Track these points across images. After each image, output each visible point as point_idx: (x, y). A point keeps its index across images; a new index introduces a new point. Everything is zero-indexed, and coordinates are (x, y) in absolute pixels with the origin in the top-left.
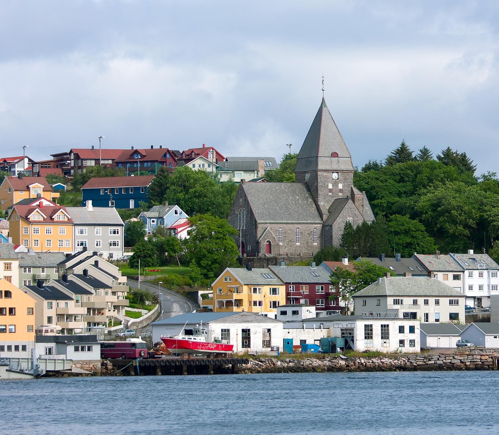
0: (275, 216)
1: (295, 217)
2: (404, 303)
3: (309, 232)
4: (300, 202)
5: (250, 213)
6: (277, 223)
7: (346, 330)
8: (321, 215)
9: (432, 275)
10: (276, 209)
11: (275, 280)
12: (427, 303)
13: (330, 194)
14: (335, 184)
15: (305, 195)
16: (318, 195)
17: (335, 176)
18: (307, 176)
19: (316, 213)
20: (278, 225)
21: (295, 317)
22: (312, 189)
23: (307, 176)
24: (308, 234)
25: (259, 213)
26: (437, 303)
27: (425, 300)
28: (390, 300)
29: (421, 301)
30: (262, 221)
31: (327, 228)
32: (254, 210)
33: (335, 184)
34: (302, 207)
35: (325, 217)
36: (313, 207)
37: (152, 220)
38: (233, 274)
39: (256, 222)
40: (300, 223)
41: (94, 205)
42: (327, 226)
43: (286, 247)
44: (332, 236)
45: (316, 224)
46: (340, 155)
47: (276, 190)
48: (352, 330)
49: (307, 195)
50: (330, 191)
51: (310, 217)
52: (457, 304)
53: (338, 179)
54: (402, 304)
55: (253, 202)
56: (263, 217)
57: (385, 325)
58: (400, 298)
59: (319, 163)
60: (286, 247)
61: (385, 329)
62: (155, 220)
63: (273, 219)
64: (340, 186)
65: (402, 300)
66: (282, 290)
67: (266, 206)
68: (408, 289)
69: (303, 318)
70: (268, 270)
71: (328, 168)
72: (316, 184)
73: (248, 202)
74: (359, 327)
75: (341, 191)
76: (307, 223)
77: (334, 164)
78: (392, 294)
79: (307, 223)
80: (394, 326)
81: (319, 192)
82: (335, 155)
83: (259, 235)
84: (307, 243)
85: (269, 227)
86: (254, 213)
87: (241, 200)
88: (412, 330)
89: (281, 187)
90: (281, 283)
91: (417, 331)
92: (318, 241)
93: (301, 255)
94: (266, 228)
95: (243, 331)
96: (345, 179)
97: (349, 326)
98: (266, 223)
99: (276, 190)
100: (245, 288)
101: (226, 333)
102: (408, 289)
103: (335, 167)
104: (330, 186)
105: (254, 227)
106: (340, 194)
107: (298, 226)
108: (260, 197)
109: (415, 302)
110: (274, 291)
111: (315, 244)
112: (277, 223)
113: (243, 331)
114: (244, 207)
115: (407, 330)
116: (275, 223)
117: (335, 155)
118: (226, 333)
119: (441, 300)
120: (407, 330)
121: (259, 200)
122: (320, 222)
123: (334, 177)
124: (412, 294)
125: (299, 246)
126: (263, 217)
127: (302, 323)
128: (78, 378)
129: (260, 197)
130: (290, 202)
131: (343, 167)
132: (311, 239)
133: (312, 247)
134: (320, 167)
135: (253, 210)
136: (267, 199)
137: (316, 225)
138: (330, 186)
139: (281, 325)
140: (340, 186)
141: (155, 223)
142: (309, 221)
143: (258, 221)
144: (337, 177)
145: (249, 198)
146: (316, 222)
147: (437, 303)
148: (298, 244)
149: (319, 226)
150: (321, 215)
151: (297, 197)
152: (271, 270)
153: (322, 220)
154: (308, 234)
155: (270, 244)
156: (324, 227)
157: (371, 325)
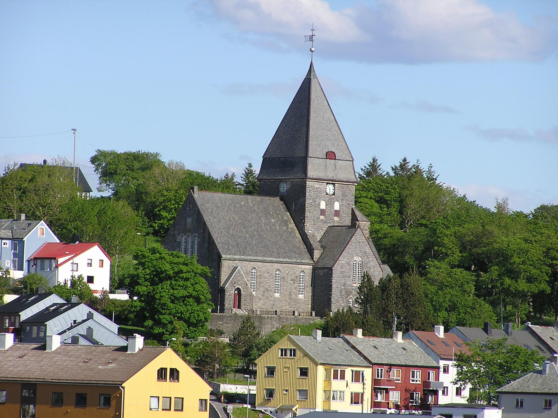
0: (246, 248)
1: (273, 252)
4: (278, 228)
8: (310, 250)
13: (322, 217)
14: (330, 204)
17: (330, 189)
19: (303, 247)
20: (251, 263)
24: (292, 280)
25: (223, 243)
27: (546, 401)
32: (215, 236)
33: (330, 204)
35: (317, 254)
36: (297, 238)
37: (4, 241)
39: (220, 257)
40: (281, 263)
43: (260, 299)
45: (304, 264)
50: (323, 212)
51: (295, 252)
52: (522, 406)
53: (334, 194)
55: (211, 224)
56: (228, 249)
59: (310, 167)
60: (260, 299)
64: (337, 206)
66: (368, 373)
70: (341, 340)
71: (321, 175)
72: (301, 200)
73: (204, 223)
75: (337, 213)
77: (329, 169)
81: (307, 214)
82: (331, 155)
83: (223, 278)
87: (189, 220)
90: (367, 364)
92: (309, 290)
94: (235, 268)
96: (344, 195)
100: (321, 370)
103: (331, 175)
104: (323, 206)
106: (336, 219)
108: (221, 217)
111: (301, 296)
117: (331, 155)
121: (220, 222)
122: (308, 261)
125: (279, 299)
126: (228, 249)
129: (221, 217)
131: (342, 176)
133: (297, 301)
137: (303, 266)
138: (323, 206)
140: (337, 206)
142: (294, 260)
143: (224, 256)
144: (332, 192)
148: (277, 295)
151: (273, 221)
152: (348, 342)
153: (312, 258)
155: (239, 294)
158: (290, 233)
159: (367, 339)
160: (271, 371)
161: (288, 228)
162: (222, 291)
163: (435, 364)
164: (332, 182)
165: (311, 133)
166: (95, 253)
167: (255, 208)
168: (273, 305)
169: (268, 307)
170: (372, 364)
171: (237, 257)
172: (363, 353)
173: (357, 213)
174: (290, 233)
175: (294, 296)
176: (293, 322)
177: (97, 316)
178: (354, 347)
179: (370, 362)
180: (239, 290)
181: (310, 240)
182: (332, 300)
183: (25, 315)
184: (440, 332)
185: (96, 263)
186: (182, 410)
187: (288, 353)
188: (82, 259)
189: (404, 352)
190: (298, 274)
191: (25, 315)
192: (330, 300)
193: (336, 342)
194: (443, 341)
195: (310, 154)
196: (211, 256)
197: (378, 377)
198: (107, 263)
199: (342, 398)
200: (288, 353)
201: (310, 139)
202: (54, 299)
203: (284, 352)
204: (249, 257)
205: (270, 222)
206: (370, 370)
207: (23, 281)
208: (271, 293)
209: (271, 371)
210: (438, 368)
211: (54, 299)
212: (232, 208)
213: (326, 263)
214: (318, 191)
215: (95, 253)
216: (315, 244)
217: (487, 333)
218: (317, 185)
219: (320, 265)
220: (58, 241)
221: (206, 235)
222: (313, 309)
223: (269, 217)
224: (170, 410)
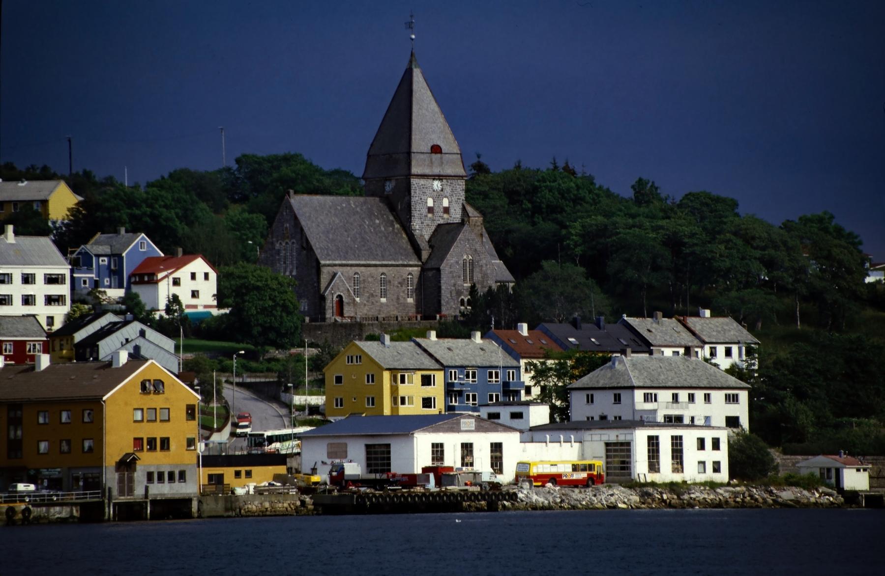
0: (347, 253)
2: (659, 398)
3: (400, 280)
4: (383, 229)
5: (306, 247)
6: (352, 265)
7: (615, 444)
8: (417, 251)
9: (693, 353)
10: (347, 242)
11: (428, 362)
12: (709, 400)
13: (430, 215)
14: (438, 197)
15: (388, 217)
16: (411, 217)
17: (437, 185)
18: (389, 187)
20: (353, 268)
21: (516, 423)
22: (400, 207)
23: (389, 187)
24: (399, 283)
25: (321, 248)
26: (707, 398)
28: (639, 395)
29: (683, 395)
30: (328, 262)
31: (430, 274)
32: (313, 242)
33: (438, 197)
34: (387, 238)
35: (425, 255)
38: (366, 350)
39: (318, 263)
41: (16, 233)
42: (432, 269)
44: (440, 288)
46: (445, 149)
47: (342, 209)
48: (628, 444)
49: (391, 218)
50: (431, 210)
51: (401, 254)
52: (592, 401)
53: (442, 190)
54: (656, 400)
55: (309, 229)
56: (328, 255)
57: (676, 437)
58: (653, 391)
59: (413, 163)
61: (677, 444)
62: (106, 259)
63: (345, 259)
65: (655, 395)
66: (439, 377)
67: (331, 236)
68: (662, 377)
69: (533, 423)
70: (412, 344)
71: (427, 171)
72: (407, 198)
73: (302, 230)
74: (640, 438)
75: (446, 210)
76: (397, 266)
78: (641, 384)
79: (397, 266)
80: (690, 438)
83: (323, 285)
84: (398, 299)
85: (339, 271)
86: (314, 248)
88: (716, 445)
89: (350, 204)
90: (437, 366)
91: (724, 446)
93: (399, 319)
94: (335, 275)
95: (434, 446)
97: (622, 438)
98: (335, 265)
99: (342, 209)
101: (438, 450)
102: (662, 377)
103: (436, 171)
104: (430, 203)
105: (314, 271)
106: (446, 216)
107: (384, 270)
108: (319, 220)
109: (675, 397)
110: (427, 381)
112: (352, 265)
113: (434, 446)
114: (293, 238)
115: (708, 444)
116: (347, 265)
117: (436, 149)
118: (438, 450)
119: (597, 395)
120: (708, 444)
122: (416, 263)
123: (435, 187)
124: (670, 384)
125: (387, 305)
126: (328, 255)
127: (530, 433)
128: (229, 519)
129: (319, 220)
130: (367, 230)
132: (404, 292)
133: (405, 305)
134: (415, 170)
135: (312, 243)
136: (330, 223)
137: (410, 269)
139: (516, 436)
140: (446, 203)
141: (106, 263)
142: (400, 262)
143: (322, 262)
144: (440, 187)
145: (303, 223)
146: (411, 263)
147: (707, 398)
148: (383, 300)
149: (416, 270)
150: (417, 251)
151: (377, 221)
153: (420, 258)
154: (399, 283)
156: (423, 270)
157: (657, 437)
158: (397, 234)
159: (441, 341)
160: (339, 380)
161: (394, 228)
162: (323, 298)
163: (515, 363)
164: (440, 177)
165: (414, 126)
166: (199, 265)
167: (358, 209)
168: (380, 311)
169: (373, 313)
170: (443, 367)
171: (337, 262)
172: (435, 355)
173: (469, 209)
174: (397, 234)
175: (402, 300)
176: (396, 328)
177: (151, 334)
178: (425, 351)
179: (442, 364)
180: (340, 297)
181: (418, 240)
182: (442, 302)
183: (80, 336)
184: (524, 329)
185: (200, 277)
186: (169, 420)
187: (355, 358)
188: (183, 273)
189: (482, 353)
190: (405, 276)
191: (80, 336)
192: (439, 302)
193: (406, 346)
194: (525, 338)
195: (414, 148)
196: (310, 264)
197: (451, 379)
198: (213, 276)
199: (411, 402)
200: (355, 358)
201: (413, 133)
202: (109, 318)
203: (350, 359)
204: (350, 262)
205: (374, 223)
206: (442, 373)
207: (122, 301)
208: (376, 299)
209: (339, 380)
210: (518, 368)
211: (109, 318)
212: (333, 212)
213: (433, 264)
214: (424, 187)
215: (199, 265)
216: (424, 245)
217: (576, 328)
218: (422, 182)
219: (429, 266)
220: (162, 255)
221: (304, 241)
222: (417, 312)
223: (373, 218)
224: (155, 421)
